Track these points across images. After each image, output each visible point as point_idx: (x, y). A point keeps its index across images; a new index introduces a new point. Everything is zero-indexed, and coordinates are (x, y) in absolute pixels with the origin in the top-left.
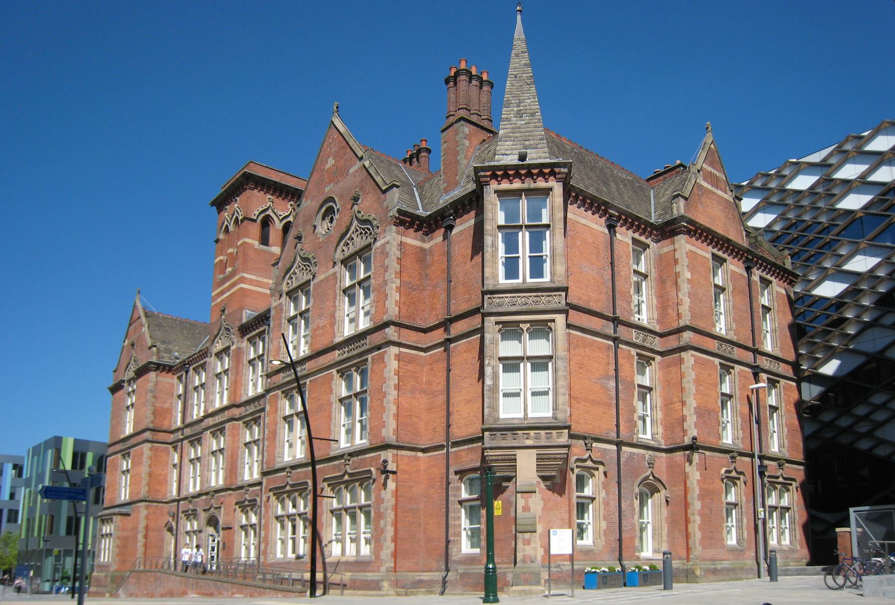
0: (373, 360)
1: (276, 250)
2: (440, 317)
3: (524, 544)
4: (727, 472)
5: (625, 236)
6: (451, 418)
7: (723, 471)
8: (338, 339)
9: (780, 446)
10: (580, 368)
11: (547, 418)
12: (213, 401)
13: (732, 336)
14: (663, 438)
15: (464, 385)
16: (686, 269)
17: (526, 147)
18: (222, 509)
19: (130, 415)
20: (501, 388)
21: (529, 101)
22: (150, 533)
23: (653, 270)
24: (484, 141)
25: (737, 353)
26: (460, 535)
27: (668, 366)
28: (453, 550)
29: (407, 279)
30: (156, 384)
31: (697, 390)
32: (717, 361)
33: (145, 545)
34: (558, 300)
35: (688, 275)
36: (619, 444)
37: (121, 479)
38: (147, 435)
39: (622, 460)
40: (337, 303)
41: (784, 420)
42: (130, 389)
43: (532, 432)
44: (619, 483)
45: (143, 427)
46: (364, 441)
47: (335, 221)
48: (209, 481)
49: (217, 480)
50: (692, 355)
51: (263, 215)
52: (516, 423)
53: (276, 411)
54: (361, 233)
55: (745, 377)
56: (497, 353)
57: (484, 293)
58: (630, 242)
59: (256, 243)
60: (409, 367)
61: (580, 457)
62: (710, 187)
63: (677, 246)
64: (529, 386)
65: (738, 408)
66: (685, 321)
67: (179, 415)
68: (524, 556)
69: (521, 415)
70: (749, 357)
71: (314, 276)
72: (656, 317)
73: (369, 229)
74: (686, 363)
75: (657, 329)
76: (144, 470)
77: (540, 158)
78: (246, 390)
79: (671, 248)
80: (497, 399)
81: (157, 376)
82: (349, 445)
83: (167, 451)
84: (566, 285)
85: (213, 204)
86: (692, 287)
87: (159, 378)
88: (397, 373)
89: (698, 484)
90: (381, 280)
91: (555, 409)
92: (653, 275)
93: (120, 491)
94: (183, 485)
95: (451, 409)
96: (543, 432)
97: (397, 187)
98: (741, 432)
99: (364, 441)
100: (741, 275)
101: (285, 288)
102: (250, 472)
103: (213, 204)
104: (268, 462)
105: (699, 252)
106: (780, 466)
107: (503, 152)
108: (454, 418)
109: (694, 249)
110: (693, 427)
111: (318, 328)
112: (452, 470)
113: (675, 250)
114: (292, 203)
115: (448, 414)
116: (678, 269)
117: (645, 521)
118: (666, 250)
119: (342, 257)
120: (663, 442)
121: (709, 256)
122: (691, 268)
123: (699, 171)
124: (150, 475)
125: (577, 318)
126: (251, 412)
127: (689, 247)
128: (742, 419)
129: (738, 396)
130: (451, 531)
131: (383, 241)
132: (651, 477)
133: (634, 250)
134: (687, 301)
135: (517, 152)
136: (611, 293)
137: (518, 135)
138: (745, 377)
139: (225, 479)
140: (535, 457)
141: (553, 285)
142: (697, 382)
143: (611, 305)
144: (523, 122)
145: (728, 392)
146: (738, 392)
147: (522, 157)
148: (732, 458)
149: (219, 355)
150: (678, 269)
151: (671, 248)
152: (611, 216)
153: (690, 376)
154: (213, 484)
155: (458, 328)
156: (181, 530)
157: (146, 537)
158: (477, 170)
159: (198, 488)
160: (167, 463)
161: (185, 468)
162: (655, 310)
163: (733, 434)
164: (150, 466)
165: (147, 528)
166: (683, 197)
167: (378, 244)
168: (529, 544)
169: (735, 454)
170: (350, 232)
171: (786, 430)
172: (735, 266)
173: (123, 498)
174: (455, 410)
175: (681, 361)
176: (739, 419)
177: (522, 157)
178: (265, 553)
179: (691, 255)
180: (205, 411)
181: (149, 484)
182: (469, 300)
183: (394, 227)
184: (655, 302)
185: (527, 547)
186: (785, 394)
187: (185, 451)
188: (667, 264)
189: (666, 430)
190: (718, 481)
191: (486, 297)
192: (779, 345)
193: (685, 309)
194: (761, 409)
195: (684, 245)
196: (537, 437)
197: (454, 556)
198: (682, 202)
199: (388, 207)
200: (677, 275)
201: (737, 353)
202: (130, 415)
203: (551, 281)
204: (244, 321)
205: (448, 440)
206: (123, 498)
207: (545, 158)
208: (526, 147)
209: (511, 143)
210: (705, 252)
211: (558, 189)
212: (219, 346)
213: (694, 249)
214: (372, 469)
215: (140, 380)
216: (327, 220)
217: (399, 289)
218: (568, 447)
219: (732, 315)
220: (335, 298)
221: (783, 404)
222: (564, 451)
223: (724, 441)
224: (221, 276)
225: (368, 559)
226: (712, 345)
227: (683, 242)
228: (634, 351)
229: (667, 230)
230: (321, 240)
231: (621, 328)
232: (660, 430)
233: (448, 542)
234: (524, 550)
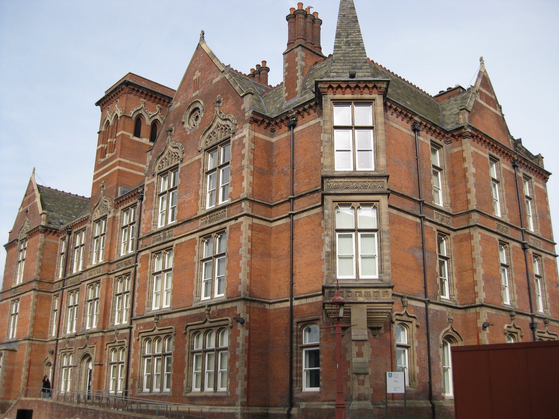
0: (230, 229)
1: (145, 141)
2: (284, 196)
3: (359, 385)
4: (508, 327)
5: (425, 138)
6: (294, 278)
7: (506, 326)
8: (200, 213)
9: (545, 308)
10: (397, 240)
11: (375, 279)
12: (91, 259)
13: (507, 219)
14: (458, 299)
15: (305, 251)
16: (472, 165)
17: (353, 68)
18: (95, 348)
19: (22, 267)
20: (337, 254)
21: (354, 34)
22: (32, 368)
23: (446, 166)
24: (316, 63)
25: (510, 233)
26: (301, 375)
27: (461, 240)
28: (296, 389)
29: (259, 166)
30: (44, 245)
31: (484, 261)
32: (497, 237)
33: (28, 378)
34: (385, 185)
35: (473, 170)
36: (427, 303)
37: (10, 320)
38: (34, 285)
39: (430, 316)
40: (201, 183)
41: (546, 286)
42: (22, 247)
43: (363, 291)
44: (428, 335)
45: (32, 279)
46: (222, 295)
47: (200, 119)
48: (84, 325)
49: (92, 324)
50: (479, 233)
51: (136, 114)
52: (351, 283)
53: (147, 268)
54: (222, 129)
55: (517, 252)
56: (334, 226)
57: (323, 178)
58: (429, 143)
59: (131, 135)
60: (260, 235)
61: (399, 313)
62: (484, 104)
63: (464, 147)
64: (360, 254)
65: (514, 276)
66: (473, 206)
67: (61, 270)
68: (359, 394)
69: (354, 277)
70: (518, 236)
71: (182, 161)
72: (449, 201)
73: (228, 126)
74: (475, 239)
75: (451, 212)
76: (30, 315)
77: (364, 76)
78: (119, 251)
79: (460, 149)
80: (335, 263)
81: (45, 236)
82: (209, 298)
83: (49, 298)
84: (387, 174)
85: (98, 104)
86: (476, 179)
87: (47, 240)
88: (251, 240)
89: (488, 337)
90: (238, 165)
91: (381, 271)
92: (446, 170)
93: (8, 331)
94: (62, 329)
95: (294, 270)
96: (381, 291)
97: (252, 94)
98: (516, 296)
99: (222, 295)
100: (510, 172)
101: (157, 171)
102: (120, 318)
103: (98, 104)
104: (138, 310)
105: (481, 153)
106: (546, 323)
107: (336, 71)
108: (297, 278)
109: (476, 150)
110: (482, 291)
111: (184, 202)
112: (295, 321)
113: (463, 151)
114: (159, 105)
115: (292, 275)
116: (466, 165)
117: (446, 367)
118: (455, 150)
119: (206, 147)
120: (458, 302)
121: (487, 156)
122: (475, 164)
123: (477, 92)
124: (35, 318)
125: (397, 202)
126: (128, 269)
127: (473, 149)
128: (517, 285)
129: (513, 266)
130: (294, 372)
131: (240, 135)
132: (451, 331)
133: (432, 149)
134: (473, 190)
135: (348, 71)
136: (416, 182)
137: (348, 59)
138: (517, 252)
139: (98, 324)
140: (366, 311)
141: (376, 174)
142: (484, 255)
143: (417, 191)
144: (351, 50)
145: (505, 263)
146: (512, 263)
147: (352, 76)
148: (512, 316)
149: (98, 221)
150: (466, 165)
151: (460, 149)
152: (416, 122)
153: (478, 249)
154: (88, 328)
155: (300, 204)
156: (58, 365)
157: (29, 370)
158: (317, 83)
159: (74, 331)
160: (49, 309)
161: (64, 313)
162: (448, 197)
163: (511, 297)
164: (35, 311)
165: (30, 363)
166: (467, 110)
167: (236, 137)
168: (363, 384)
169: (514, 313)
170: (213, 127)
171: (547, 294)
172: (505, 165)
173: (11, 337)
174: (297, 271)
175: (470, 237)
176: (515, 285)
177: (352, 76)
178: (133, 387)
179: (475, 154)
180: (84, 267)
181: (33, 326)
182: (309, 184)
183: (248, 124)
184: (448, 190)
185: (361, 387)
186: (546, 266)
187: (65, 299)
188: (455, 161)
189: (461, 292)
190: (502, 334)
191: (325, 181)
192: (539, 227)
193: (472, 197)
194: (530, 278)
195: (469, 147)
196: (367, 295)
197: (296, 395)
198: (467, 115)
199: (244, 109)
200: (465, 170)
201: (510, 233)
202: (22, 267)
203: (376, 170)
204: (119, 195)
205: (292, 296)
206: (11, 337)
207: (368, 76)
208: (353, 68)
209: (342, 64)
210: (485, 153)
211: (379, 100)
212: (97, 215)
213: (476, 150)
214: (229, 318)
215: (31, 240)
216: (193, 117)
217: (253, 174)
218: (393, 303)
219: (505, 203)
220: (199, 179)
221: (545, 274)
222: (389, 307)
223: (505, 303)
224: (102, 160)
225: (225, 394)
226: (493, 225)
227: (469, 144)
228: (435, 228)
229: (457, 134)
230: (188, 133)
231: (427, 210)
232: (456, 292)
233: (291, 381)
234: (359, 389)
